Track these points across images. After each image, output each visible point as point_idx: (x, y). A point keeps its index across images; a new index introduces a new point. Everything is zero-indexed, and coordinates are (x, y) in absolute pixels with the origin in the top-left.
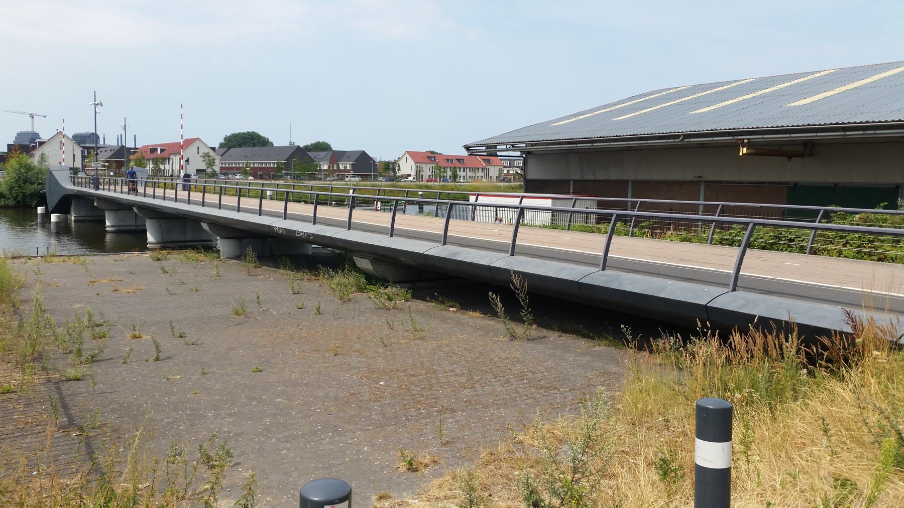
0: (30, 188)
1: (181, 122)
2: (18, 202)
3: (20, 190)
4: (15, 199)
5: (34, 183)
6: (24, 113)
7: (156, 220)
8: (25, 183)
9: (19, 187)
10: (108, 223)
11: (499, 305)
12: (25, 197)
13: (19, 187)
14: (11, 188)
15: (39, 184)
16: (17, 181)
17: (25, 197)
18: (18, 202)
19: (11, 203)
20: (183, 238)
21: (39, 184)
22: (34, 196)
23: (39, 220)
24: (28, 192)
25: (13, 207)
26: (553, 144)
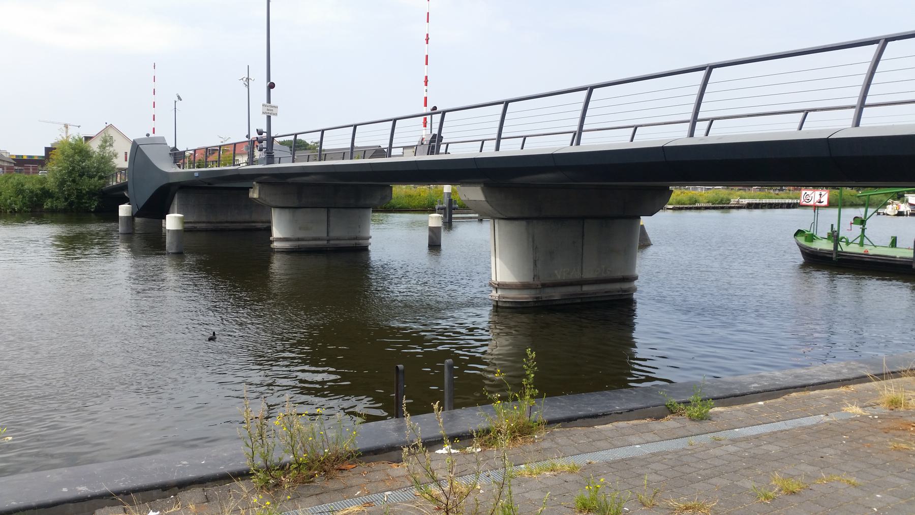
0: (88, 184)
1: (425, 49)
2: (71, 204)
3: (74, 186)
4: (66, 199)
5: (93, 177)
6: (58, 123)
7: (524, 223)
8: (81, 176)
9: (74, 181)
10: (276, 233)
11: (827, 419)
12: (80, 196)
13: (74, 181)
14: (62, 183)
15: (101, 178)
16: (70, 173)
17: (80, 196)
18: (71, 204)
19: (61, 204)
20: (575, 275)
21: (101, 178)
22: (94, 194)
23: (121, 228)
24: (85, 188)
25: (64, 211)
26: (471, 218)
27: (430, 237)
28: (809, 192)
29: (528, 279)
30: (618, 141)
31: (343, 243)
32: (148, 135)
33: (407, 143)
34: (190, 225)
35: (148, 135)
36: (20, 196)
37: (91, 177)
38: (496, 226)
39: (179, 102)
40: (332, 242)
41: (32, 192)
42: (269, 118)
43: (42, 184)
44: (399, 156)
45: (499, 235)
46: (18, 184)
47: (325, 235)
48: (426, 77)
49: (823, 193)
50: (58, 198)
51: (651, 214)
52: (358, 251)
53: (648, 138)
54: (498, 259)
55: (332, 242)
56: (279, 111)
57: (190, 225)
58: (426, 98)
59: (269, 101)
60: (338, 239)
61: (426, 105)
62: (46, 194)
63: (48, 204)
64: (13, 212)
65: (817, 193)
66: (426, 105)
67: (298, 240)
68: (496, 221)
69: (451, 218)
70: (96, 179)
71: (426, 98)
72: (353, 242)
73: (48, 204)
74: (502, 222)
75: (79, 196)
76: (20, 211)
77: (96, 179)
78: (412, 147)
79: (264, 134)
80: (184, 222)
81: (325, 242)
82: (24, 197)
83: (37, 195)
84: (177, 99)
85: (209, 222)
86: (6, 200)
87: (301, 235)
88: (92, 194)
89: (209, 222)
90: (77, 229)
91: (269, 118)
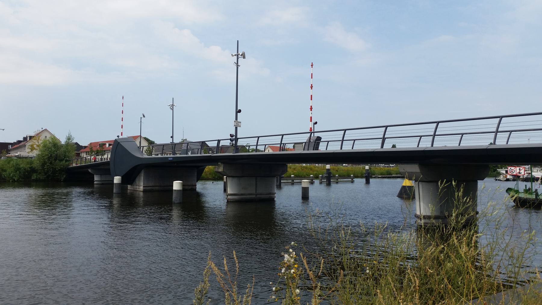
0: (60, 165)
4: (46, 174)
8: (55, 160)
14: (44, 164)
15: (66, 161)
19: (42, 177)
27: (303, 193)
28: (513, 168)
29: (435, 214)
30: (451, 143)
31: (263, 197)
32: (118, 136)
33: (295, 141)
34: (150, 188)
35: (118, 136)
36: (18, 172)
37: (61, 160)
38: (420, 187)
39: (143, 119)
40: (258, 196)
41: (25, 169)
42: (236, 128)
43: (31, 165)
44: (290, 149)
45: (423, 192)
46: (17, 164)
47: (254, 192)
48: (311, 106)
49: (521, 168)
50: (40, 173)
51: (482, 179)
52: (271, 201)
53: (470, 143)
54: (422, 204)
55: (258, 196)
56: (242, 125)
57: (150, 188)
58: (311, 117)
59: (236, 119)
60: (261, 194)
61: (311, 121)
62: (33, 170)
63: (34, 177)
64: (14, 181)
65: (518, 168)
66: (311, 121)
67: (242, 195)
68: (420, 183)
69: (280, 183)
70: (64, 162)
71: (311, 117)
72: (268, 196)
73: (34, 177)
74: (424, 183)
75: (55, 172)
76: (17, 181)
77: (64, 162)
78: (302, 143)
79: (234, 137)
80: (183, 185)
81: (254, 196)
82: (20, 172)
83: (27, 171)
84: (142, 116)
85: (160, 186)
86: (10, 175)
87: (243, 192)
88: (61, 170)
89: (160, 186)
90: (51, 191)
91: (236, 128)
